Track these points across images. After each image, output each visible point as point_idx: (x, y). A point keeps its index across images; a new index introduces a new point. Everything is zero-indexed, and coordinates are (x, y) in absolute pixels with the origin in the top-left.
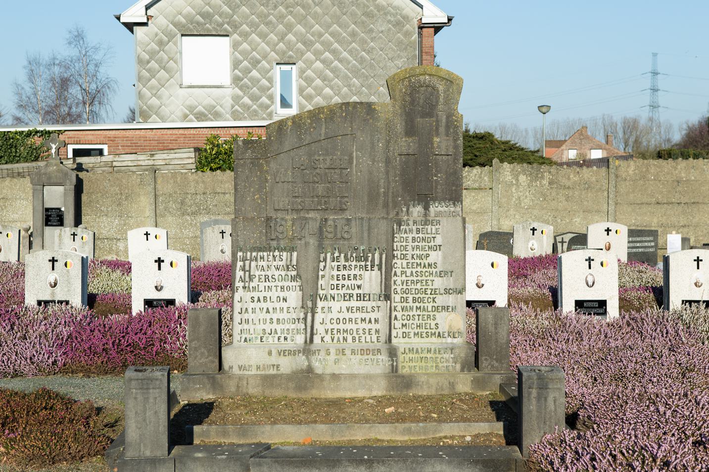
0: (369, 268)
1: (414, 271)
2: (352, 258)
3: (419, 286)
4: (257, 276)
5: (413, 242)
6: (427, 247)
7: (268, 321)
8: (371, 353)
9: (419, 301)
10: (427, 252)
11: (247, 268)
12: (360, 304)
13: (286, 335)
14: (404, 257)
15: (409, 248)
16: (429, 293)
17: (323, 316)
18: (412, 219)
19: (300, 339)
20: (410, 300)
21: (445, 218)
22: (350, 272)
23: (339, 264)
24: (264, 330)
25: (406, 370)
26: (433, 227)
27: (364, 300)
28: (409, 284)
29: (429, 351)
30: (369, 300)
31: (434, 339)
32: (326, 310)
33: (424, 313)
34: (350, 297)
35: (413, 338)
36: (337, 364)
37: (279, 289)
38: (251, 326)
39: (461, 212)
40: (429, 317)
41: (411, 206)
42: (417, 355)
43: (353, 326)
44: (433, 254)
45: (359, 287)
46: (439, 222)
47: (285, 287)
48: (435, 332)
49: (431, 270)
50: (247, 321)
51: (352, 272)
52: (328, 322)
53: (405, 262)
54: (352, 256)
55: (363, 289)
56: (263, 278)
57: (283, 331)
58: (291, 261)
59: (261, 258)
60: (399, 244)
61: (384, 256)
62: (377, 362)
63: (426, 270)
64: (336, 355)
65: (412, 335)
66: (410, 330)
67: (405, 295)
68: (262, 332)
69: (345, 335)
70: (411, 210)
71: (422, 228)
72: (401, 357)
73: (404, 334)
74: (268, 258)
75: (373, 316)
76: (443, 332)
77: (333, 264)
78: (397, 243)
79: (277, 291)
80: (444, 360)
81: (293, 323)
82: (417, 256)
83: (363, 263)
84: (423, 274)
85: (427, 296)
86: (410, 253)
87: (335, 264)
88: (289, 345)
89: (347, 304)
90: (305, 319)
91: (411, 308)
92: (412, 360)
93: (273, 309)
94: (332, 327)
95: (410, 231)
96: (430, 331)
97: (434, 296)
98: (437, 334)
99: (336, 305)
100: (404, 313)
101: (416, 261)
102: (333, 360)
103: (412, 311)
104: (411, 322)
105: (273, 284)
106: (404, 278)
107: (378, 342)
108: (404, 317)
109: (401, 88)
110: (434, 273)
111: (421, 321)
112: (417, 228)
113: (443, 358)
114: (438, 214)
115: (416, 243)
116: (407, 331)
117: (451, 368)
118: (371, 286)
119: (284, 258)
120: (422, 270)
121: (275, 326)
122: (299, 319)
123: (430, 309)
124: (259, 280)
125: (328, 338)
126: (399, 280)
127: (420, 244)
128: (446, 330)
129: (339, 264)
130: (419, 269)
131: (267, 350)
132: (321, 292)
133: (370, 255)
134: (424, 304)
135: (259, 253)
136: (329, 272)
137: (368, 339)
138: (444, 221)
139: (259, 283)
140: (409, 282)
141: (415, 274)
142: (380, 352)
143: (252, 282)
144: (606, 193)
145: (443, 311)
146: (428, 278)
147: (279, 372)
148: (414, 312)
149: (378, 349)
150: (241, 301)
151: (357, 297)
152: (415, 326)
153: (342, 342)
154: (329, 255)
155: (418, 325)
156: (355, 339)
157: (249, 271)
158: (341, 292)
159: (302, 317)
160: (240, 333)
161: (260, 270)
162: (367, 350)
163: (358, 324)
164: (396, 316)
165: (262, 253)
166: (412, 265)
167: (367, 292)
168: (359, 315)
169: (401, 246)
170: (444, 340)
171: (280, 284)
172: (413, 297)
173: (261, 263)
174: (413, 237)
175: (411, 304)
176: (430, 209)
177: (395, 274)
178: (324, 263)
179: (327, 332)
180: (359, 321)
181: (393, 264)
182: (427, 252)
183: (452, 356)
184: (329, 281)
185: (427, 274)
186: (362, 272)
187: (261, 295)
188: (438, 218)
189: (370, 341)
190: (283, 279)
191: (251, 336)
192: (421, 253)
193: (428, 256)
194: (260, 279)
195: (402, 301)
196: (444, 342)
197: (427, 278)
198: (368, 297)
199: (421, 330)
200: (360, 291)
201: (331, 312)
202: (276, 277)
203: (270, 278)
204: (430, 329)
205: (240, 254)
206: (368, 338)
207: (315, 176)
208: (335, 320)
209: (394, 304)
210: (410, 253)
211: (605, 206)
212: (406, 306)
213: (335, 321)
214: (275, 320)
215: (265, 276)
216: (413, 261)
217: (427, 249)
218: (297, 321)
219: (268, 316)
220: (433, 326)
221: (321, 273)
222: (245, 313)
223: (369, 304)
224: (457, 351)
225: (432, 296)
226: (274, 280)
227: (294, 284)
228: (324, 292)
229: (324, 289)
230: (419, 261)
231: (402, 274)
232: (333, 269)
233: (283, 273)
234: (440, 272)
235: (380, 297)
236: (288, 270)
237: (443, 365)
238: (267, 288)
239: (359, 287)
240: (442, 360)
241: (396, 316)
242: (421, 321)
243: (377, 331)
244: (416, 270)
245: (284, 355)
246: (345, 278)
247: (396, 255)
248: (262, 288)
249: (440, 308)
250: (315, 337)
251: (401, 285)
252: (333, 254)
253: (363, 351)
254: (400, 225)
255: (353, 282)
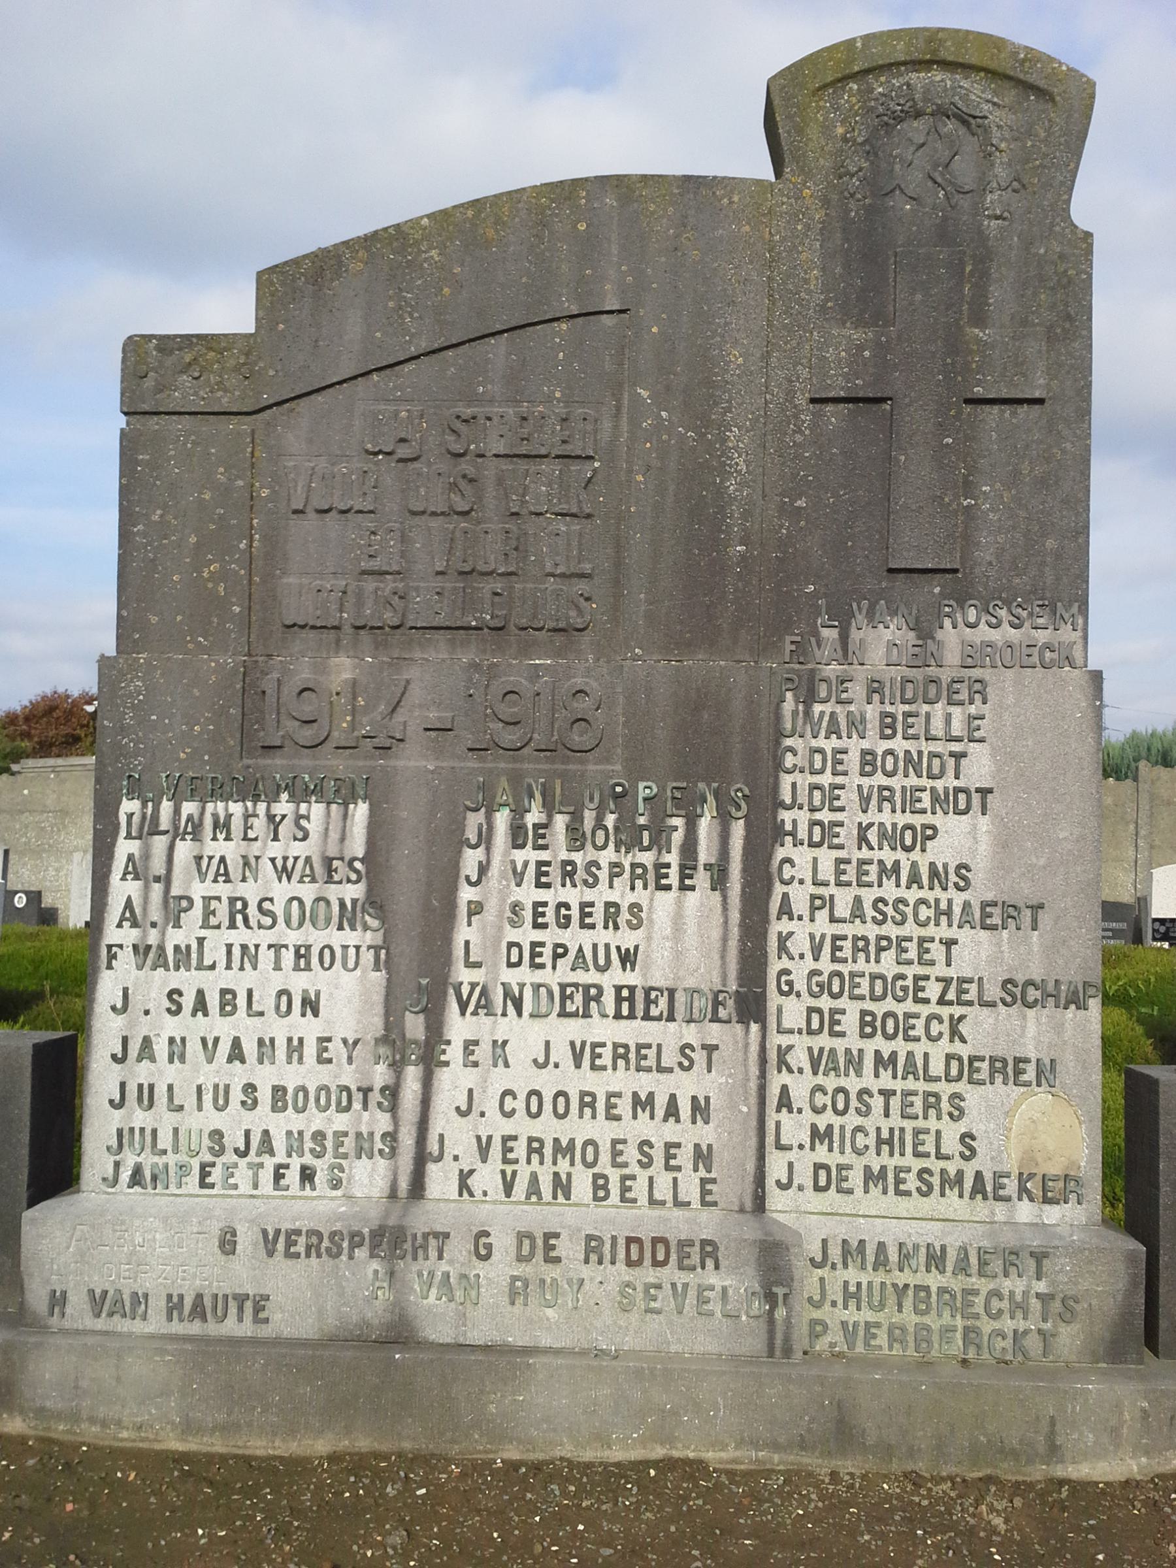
0: (673, 879)
1: (868, 896)
2: (600, 834)
3: (888, 964)
4: (198, 904)
5: (863, 774)
6: (926, 797)
7: (237, 1095)
8: (674, 1257)
9: (890, 1030)
10: (928, 819)
11: (158, 866)
12: (630, 1032)
13: (308, 1159)
14: (827, 835)
15: (848, 797)
16: (934, 999)
17: (469, 1078)
18: (861, 674)
19: (369, 1179)
20: (850, 1022)
21: (1010, 673)
22: (589, 895)
23: (544, 856)
24: (217, 1135)
25: (828, 1338)
26: (956, 711)
27: (647, 1017)
28: (847, 952)
29: (936, 1259)
30: (671, 1018)
31: (954, 1204)
32: (483, 1053)
33: (911, 1084)
34: (587, 999)
35: (859, 1192)
36: (520, 1300)
37: (288, 957)
38: (163, 1120)
39: (1078, 648)
40: (932, 1102)
41: (860, 618)
42: (879, 1278)
43: (602, 1131)
44: (951, 825)
45: (628, 958)
46: (979, 689)
47: (315, 952)
48: (960, 1174)
49: (943, 897)
50: (147, 1097)
51: (601, 895)
52: (491, 1106)
53: (827, 858)
54: (599, 824)
55: (647, 967)
56: (222, 909)
57: (295, 1141)
58: (343, 839)
59: (216, 825)
60: (804, 781)
61: (738, 830)
62: (702, 1301)
63: (922, 894)
64: (520, 1259)
65: (856, 1178)
66: (849, 1158)
67: (825, 1003)
68: (206, 1142)
69: (563, 1165)
70: (855, 635)
71: (907, 715)
72: (809, 1281)
73: (823, 1174)
74: (247, 827)
75: (686, 1086)
76: (998, 1175)
77: (519, 856)
78: (797, 777)
79: (278, 967)
80: (1005, 1305)
81: (341, 1109)
82: (883, 835)
83: (647, 858)
84: (909, 910)
85: (925, 1010)
86: (852, 818)
87: (528, 855)
88: (318, 1207)
89: (574, 1029)
90: (392, 1092)
91: (854, 1062)
92: (857, 1296)
93: (261, 1042)
94: (507, 1127)
95: (852, 724)
96: (936, 1165)
97: (957, 1011)
98: (968, 1183)
99: (525, 1035)
100: (820, 1079)
101: (876, 855)
102: (505, 1282)
103: (859, 1074)
104: (852, 1120)
105: (265, 938)
106: (822, 925)
107: (704, 1203)
108: (820, 1100)
109: (830, 125)
110: (957, 910)
111: (896, 1121)
112: (884, 715)
113: (996, 1294)
114: (973, 657)
115: (880, 779)
116: (833, 1159)
117: (1033, 1344)
118: (678, 955)
119: (314, 826)
120: (902, 893)
121: (263, 1118)
122: (366, 1091)
123: (937, 1067)
124: (206, 918)
125: (487, 1178)
126: (801, 934)
127: (896, 783)
128: (1011, 1165)
129: (544, 856)
130: (890, 891)
131: (215, 1228)
132: (464, 976)
133: (678, 822)
134: (911, 1046)
135: (210, 807)
136: (501, 886)
137: (663, 1191)
138: (1004, 684)
139: (203, 933)
140: (847, 945)
141: (870, 912)
142: (714, 1255)
143: (177, 925)
144: (1132, 827)
145: (999, 1079)
146: (931, 931)
147: (265, 1331)
148: (868, 1080)
149: (704, 1243)
150: (125, 1008)
151: (619, 1000)
152: (871, 1141)
153: (547, 1193)
154: (502, 819)
155: (885, 1134)
156: (605, 1188)
157: (167, 880)
158: (552, 978)
159: (378, 1083)
160: (114, 1142)
161: (211, 876)
162: (655, 1241)
163: (618, 1118)
164: (785, 1089)
165: (220, 805)
166: (861, 873)
167: (658, 979)
168: (624, 1081)
169: (815, 787)
170: (1001, 1211)
171: (293, 938)
172: (863, 1013)
173: (216, 848)
174: (864, 753)
175: (853, 1042)
176: (939, 635)
177: (786, 910)
178: (481, 850)
179: (484, 1151)
180: (624, 1107)
181: (775, 863)
182: (928, 819)
183: (1041, 1287)
184: (500, 929)
185: (924, 913)
186: (641, 895)
187: (213, 983)
188: (976, 673)
189: (669, 1198)
190: (307, 917)
191: (160, 1161)
192: (902, 819)
193: (930, 833)
194: (208, 913)
195: (815, 1025)
196: (1000, 1216)
197: (923, 932)
198: (663, 1002)
199: (897, 1160)
200: (632, 978)
201: (509, 1061)
202: (278, 908)
203: (252, 911)
204: (939, 1156)
205: (129, 806)
206: (663, 1182)
207: (454, 486)
208: (522, 1097)
209: (776, 1040)
210: (852, 818)
211: (1131, 853)
212: (832, 1051)
213: (520, 1104)
214: (264, 1095)
215: (232, 901)
216: (865, 853)
217: (926, 802)
218: (358, 1097)
219: (238, 1076)
220: (951, 1144)
221: (466, 894)
222: (140, 1059)
223: (668, 1036)
224: (1061, 1266)
225: (945, 1011)
226: (268, 921)
227: (351, 937)
228: (477, 975)
229: (478, 965)
230: (888, 856)
231: (813, 909)
232: (519, 878)
233: (308, 892)
234: (984, 905)
235: (716, 1004)
236: (330, 880)
237: (997, 1325)
238: (236, 952)
239: (628, 958)
240: (995, 1304)
241: (785, 1089)
242: (896, 1121)
243: (703, 1156)
244: (875, 892)
245: (288, 1255)
246: (568, 918)
247: (788, 827)
248: (214, 953)
249: (985, 1065)
250: (432, 1169)
251: (809, 956)
252: (519, 812)
253: (640, 1250)
254: (810, 698)
255: (602, 936)
